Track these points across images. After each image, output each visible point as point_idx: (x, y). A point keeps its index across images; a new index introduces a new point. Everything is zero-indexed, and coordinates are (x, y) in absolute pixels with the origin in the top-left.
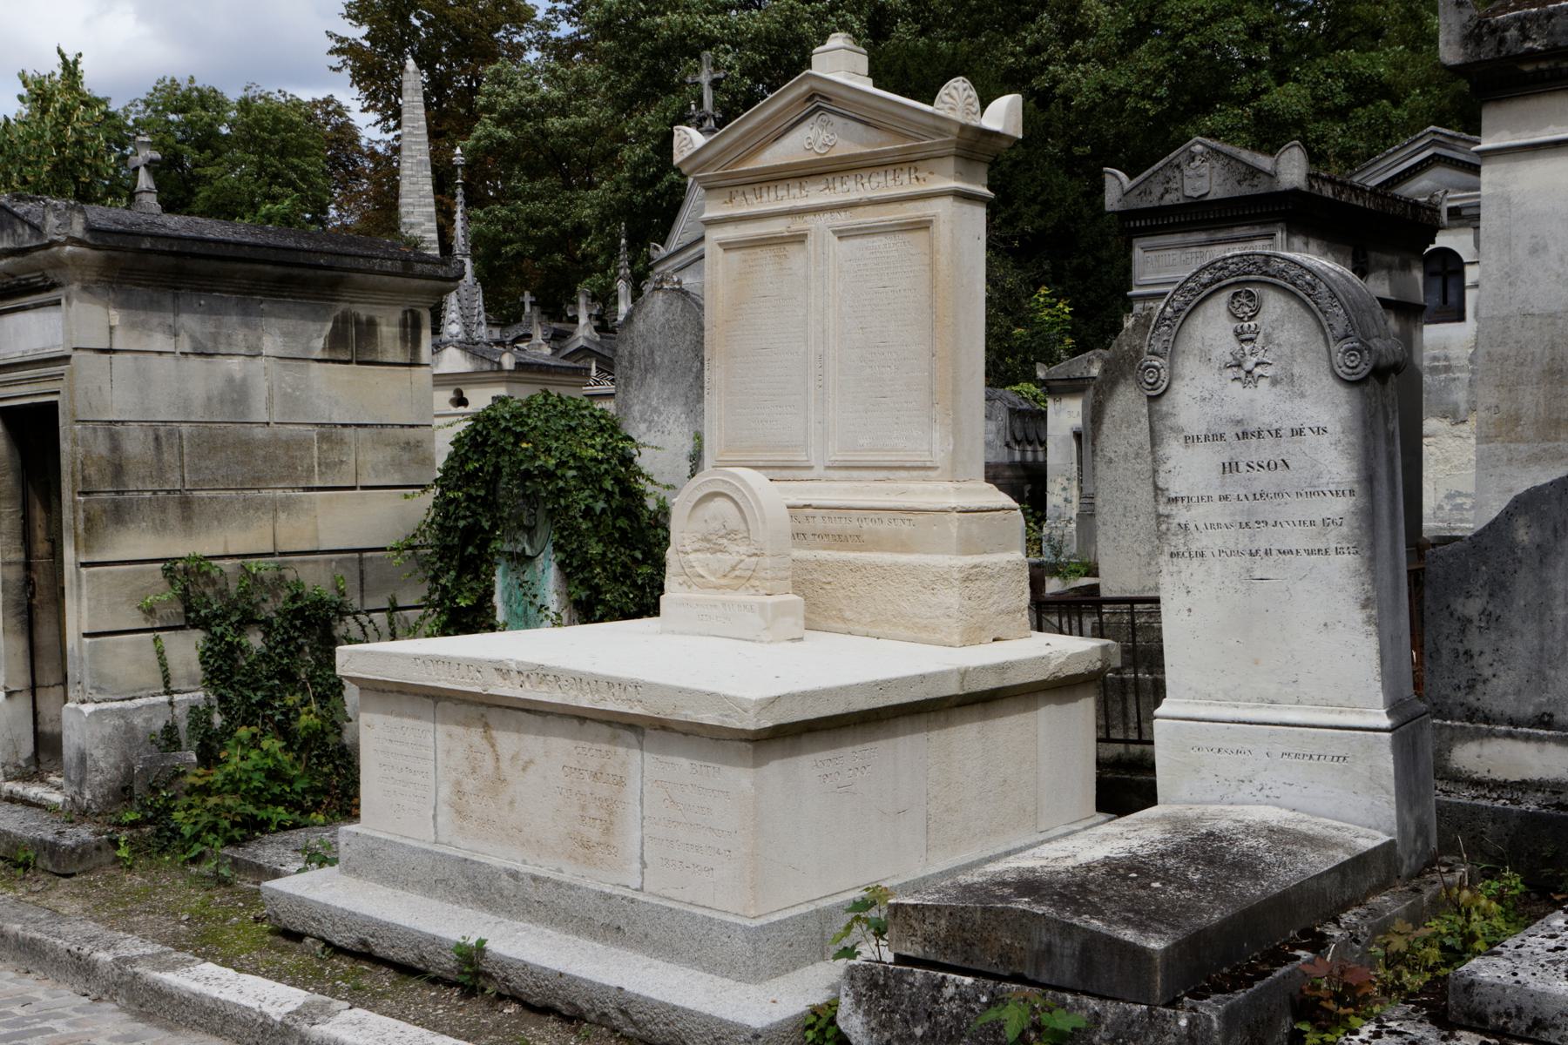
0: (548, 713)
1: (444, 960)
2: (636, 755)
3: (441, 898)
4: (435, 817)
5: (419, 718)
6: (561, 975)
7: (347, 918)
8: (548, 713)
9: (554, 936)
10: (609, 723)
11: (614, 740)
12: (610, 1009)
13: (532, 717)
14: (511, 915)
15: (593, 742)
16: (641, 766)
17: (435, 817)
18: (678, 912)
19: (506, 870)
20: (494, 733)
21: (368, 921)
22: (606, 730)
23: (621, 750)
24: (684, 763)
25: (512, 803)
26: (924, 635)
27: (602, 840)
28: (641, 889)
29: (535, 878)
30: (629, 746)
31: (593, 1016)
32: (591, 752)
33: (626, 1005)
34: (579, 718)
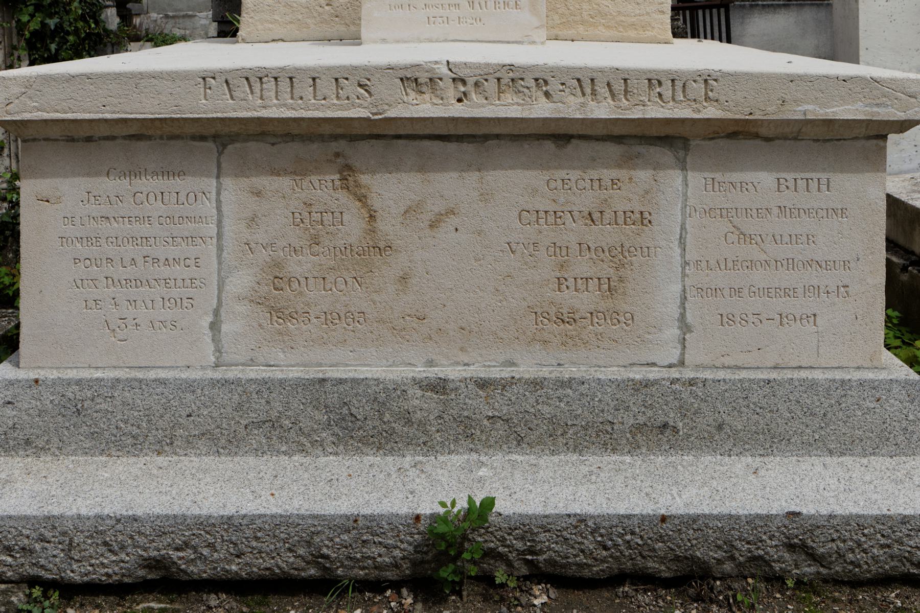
0: (486, 137)
1: (375, 551)
2: (673, 179)
3: (258, 452)
4: (215, 326)
5: (181, 174)
6: (664, 519)
7: (106, 532)
8: (486, 137)
9: (125, 467)
10: (619, 139)
11: (628, 162)
12: (773, 550)
13: (452, 147)
14: (428, 447)
15: (584, 169)
16: (677, 192)
17: (215, 326)
18: (780, 384)
19: (417, 382)
20: (364, 179)
21: (165, 526)
22: (613, 150)
23: (643, 175)
24: (765, 179)
25: (404, 279)
26: (632, 34)
27: (602, 306)
28: (682, 363)
29: (483, 384)
30: (657, 167)
31: (728, 567)
32: (575, 185)
33: (799, 535)
34: (559, 139)
